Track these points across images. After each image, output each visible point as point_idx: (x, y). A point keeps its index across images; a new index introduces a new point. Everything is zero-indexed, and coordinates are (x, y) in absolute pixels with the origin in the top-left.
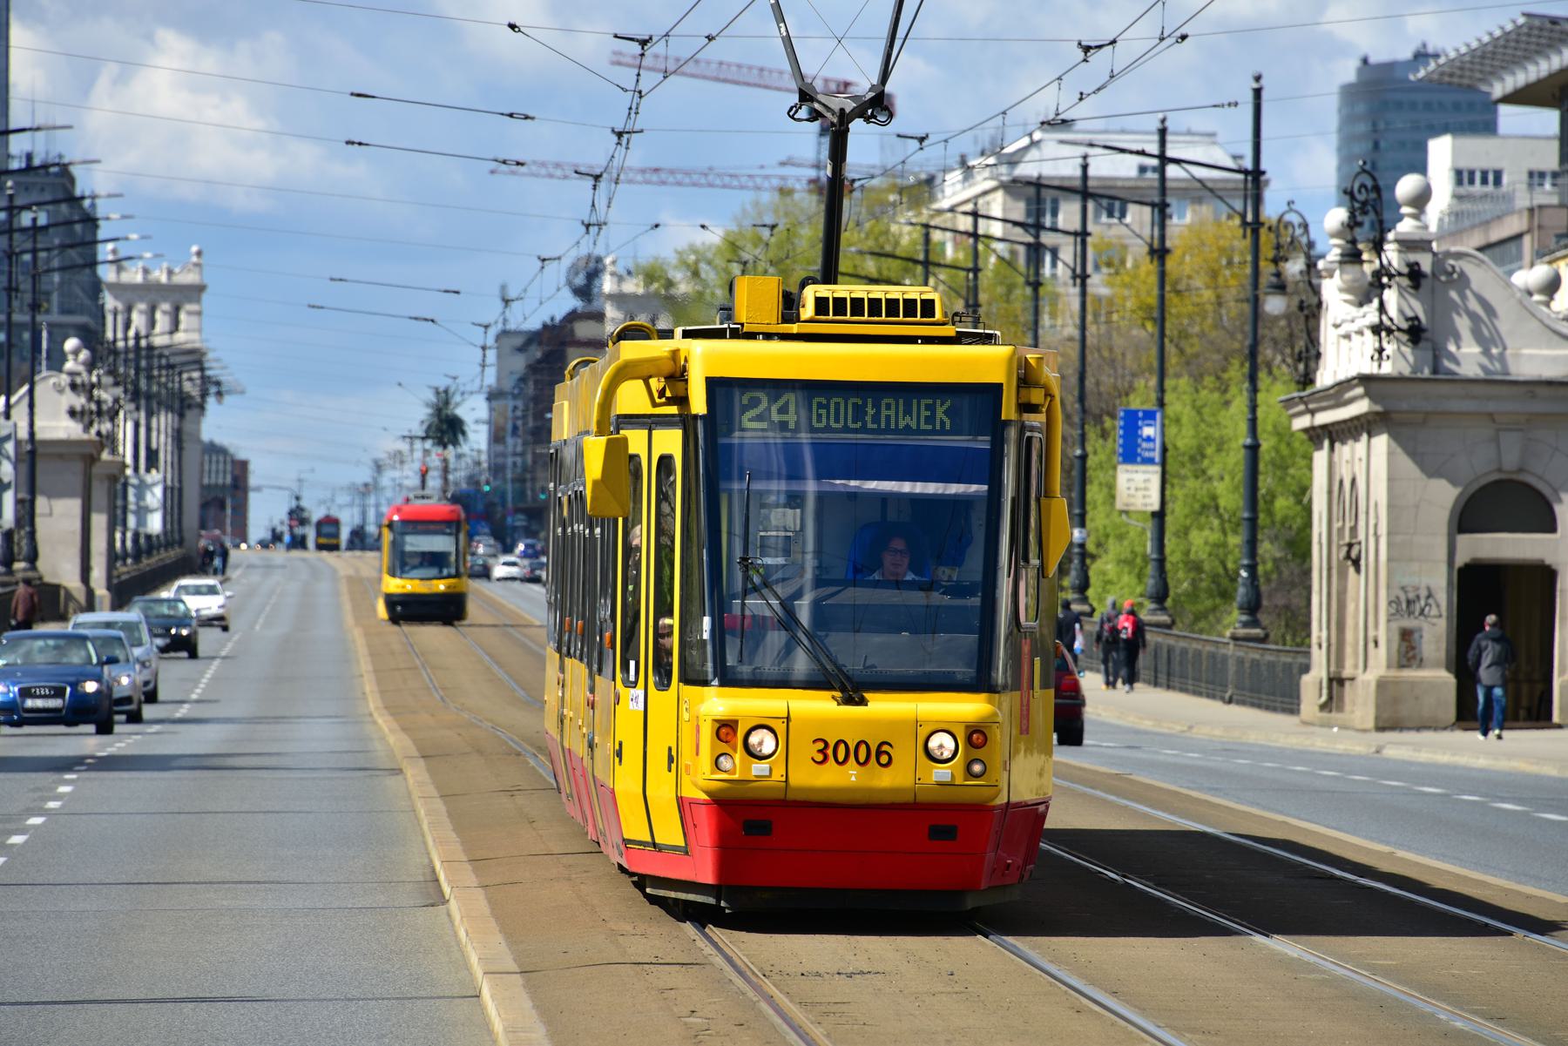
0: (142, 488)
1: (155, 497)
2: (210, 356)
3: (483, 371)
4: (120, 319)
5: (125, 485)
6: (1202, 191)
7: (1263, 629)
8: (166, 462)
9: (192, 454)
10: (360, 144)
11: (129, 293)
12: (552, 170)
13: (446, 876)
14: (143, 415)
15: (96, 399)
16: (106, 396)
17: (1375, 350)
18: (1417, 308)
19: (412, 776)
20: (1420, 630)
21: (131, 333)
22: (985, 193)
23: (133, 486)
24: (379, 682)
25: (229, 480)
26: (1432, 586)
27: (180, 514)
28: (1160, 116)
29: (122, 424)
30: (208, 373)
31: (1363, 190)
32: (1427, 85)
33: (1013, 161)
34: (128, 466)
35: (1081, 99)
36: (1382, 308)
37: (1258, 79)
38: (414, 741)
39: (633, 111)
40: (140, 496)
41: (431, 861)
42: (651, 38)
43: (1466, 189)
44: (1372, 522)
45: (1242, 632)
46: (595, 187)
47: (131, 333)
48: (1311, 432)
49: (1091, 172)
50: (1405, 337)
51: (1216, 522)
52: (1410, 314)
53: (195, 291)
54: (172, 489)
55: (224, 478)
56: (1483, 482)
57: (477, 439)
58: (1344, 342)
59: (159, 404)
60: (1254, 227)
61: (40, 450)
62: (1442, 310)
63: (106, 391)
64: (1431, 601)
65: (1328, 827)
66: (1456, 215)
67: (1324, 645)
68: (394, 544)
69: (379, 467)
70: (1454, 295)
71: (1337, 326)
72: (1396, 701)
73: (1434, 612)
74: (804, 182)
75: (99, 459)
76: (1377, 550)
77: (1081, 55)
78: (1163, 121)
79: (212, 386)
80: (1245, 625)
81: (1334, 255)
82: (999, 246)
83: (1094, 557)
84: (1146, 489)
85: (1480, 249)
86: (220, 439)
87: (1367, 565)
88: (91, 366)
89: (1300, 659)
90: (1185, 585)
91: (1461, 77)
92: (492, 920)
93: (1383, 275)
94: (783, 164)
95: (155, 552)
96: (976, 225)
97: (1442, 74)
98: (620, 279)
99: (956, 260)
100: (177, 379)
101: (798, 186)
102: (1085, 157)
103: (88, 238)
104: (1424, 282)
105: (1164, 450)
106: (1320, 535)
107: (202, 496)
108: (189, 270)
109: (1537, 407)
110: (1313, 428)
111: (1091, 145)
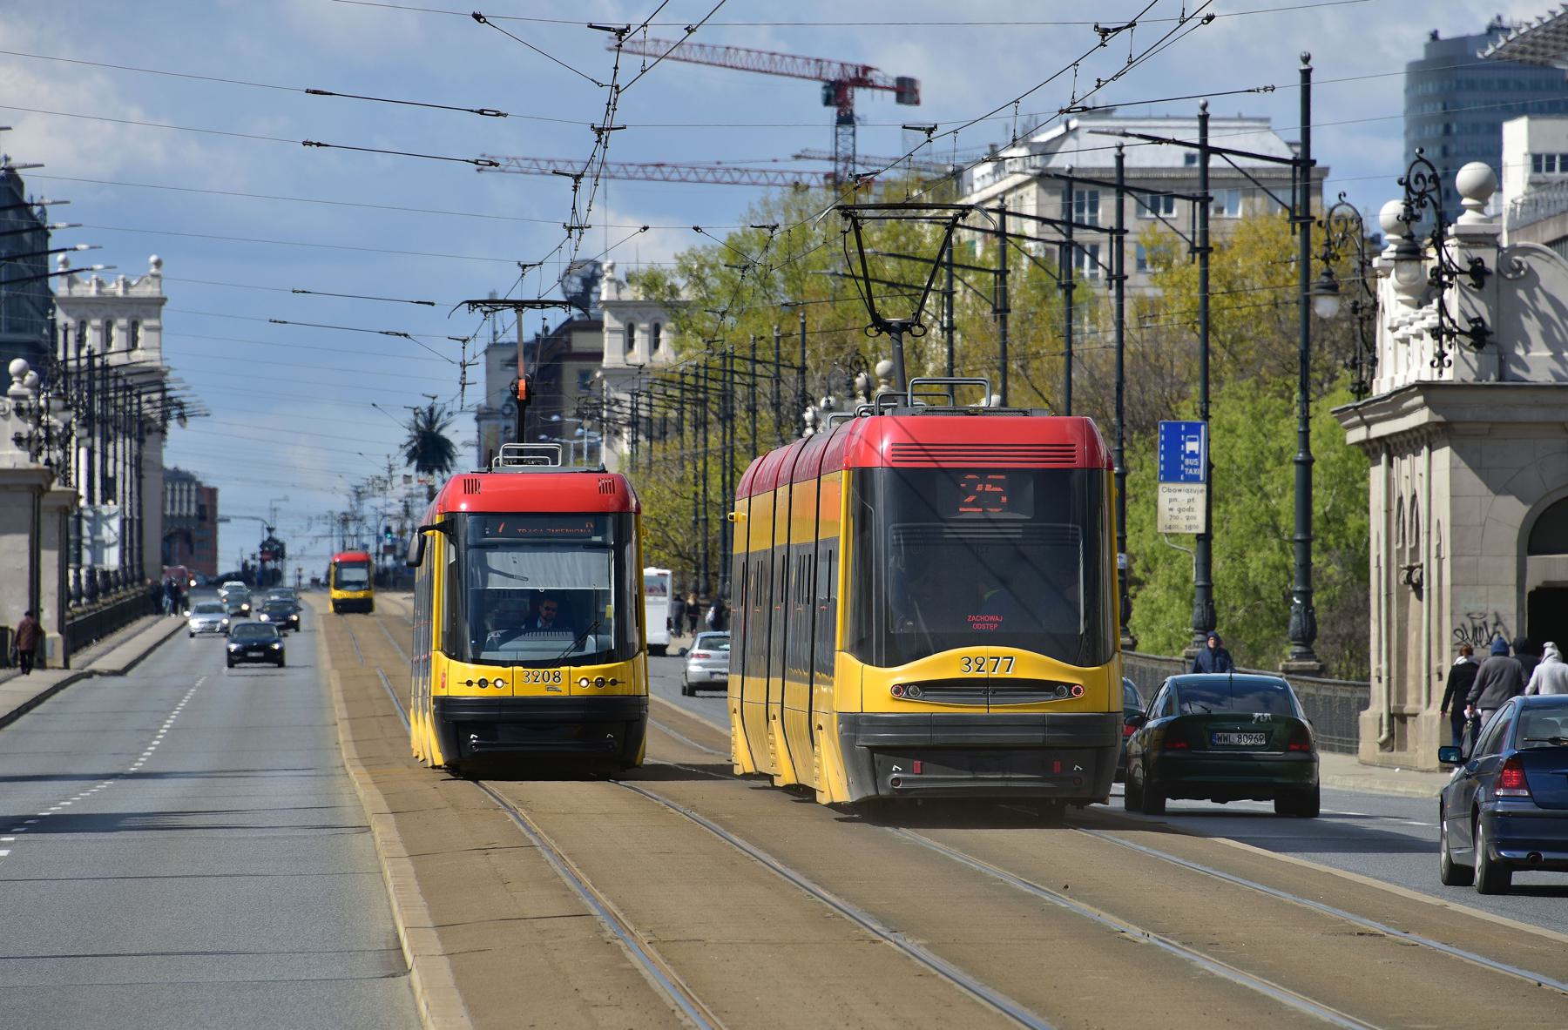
0: (98, 520)
1: (111, 530)
2: (171, 375)
3: (463, 389)
4: (72, 336)
5: (79, 517)
6: (1250, 183)
7: (1319, 661)
8: (124, 492)
9: (152, 481)
10: (319, 145)
11: (83, 308)
12: (532, 167)
13: (409, 945)
14: (98, 441)
15: (44, 424)
16: (56, 421)
17: (1435, 355)
18: (1482, 309)
19: (380, 834)
21: (84, 353)
22: (1018, 186)
23: (88, 519)
24: (354, 729)
25: (193, 510)
26: (1501, 612)
27: (140, 548)
28: (1202, 101)
29: (74, 451)
30: (169, 394)
31: (1420, 180)
32: (1496, 63)
33: (1047, 151)
34: (81, 497)
35: (1098, 87)
36: (1442, 310)
37: (1306, 59)
38: (387, 796)
39: (611, 106)
40: (96, 530)
41: (395, 927)
42: (628, 28)
43: (1544, 175)
44: (1434, 543)
45: (1296, 664)
46: (575, 189)
47: (84, 353)
48: (1368, 446)
49: (1126, 163)
50: (1467, 341)
51: (1275, 542)
52: (1473, 315)
54: (131, 520)
55: (189, 509)
56: (1556, 497)
57: (466, 461)
58: (1402, 347)
59: (115, 428)
60: (1302, 218)
62: (1508, 311)
63: (56, 417)
64: (1499, 628)
65: (1377, 878)
66: (1531, 204)
67: (1384, 678)
68: (454, 571)
69: (359, 494)
70: (1521, 294)
71: (1394, 329)
74: (821, 177)
75: (48, 490)
76: (1440, 573)
77: (1099, 39)
78: (1204, 107)
79: (174, 408)
80: (1300, 657)
81: (1389, 252)
82: (1031, 245)
83: (1140, 584)
84: (1190, 509)
85: (1549, 244)
86: (185, 465)
87: (1429, 590)
88: (36, 389)
89: (1359, 694)
90: (1240, 612)
91: (1533, 53)
92: (456, 991)
93: (1443, 273)
94: (798, 157)
95: (112, 590)
96: (1003, 222)
97: (1512, 51)
98: (619, 286)
99: (984, 261)
100: (136, 401)
101: (814, 182)
102: (1120, 147)
103: (38, 249)
104: (1488, 281)
105: (1210, 466)
106: (1378, 557)
107: (163, 528)
108: (148, 283)
110: (1369, 441)
111: (1125, 135)
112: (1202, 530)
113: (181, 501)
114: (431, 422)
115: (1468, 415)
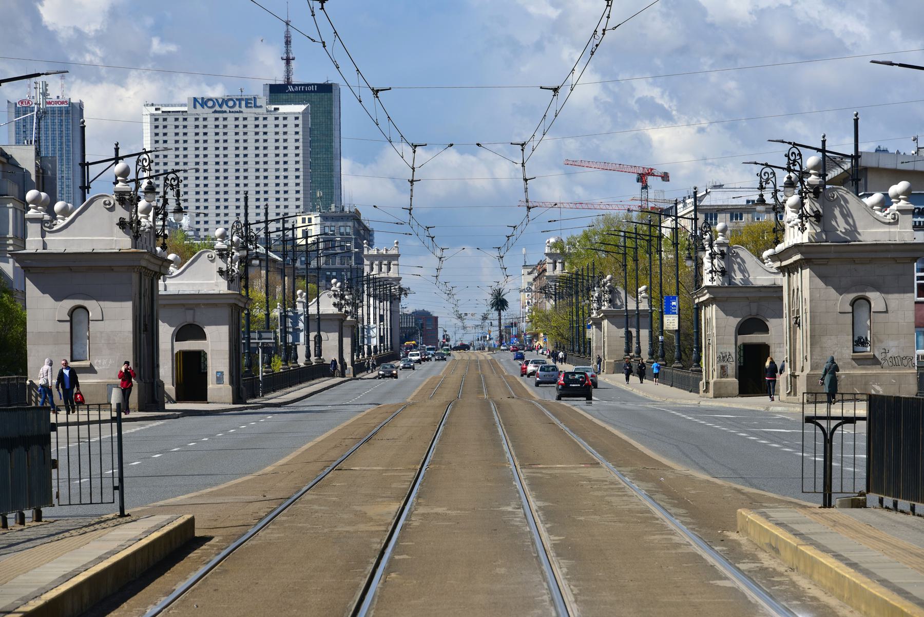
20: (727, 366)
37: (695, 189)
40: (369, 333)
53: (396, 257)
61: (321, 318)
62: (730, 264)
72: (720, 388)
73: (731, 360)
104: (725, 256)
105: (679, 310)
109: (762, 295)
112: (677, 328)
113: (409, 322)
114: (499, 294)
115: (720, 295)
